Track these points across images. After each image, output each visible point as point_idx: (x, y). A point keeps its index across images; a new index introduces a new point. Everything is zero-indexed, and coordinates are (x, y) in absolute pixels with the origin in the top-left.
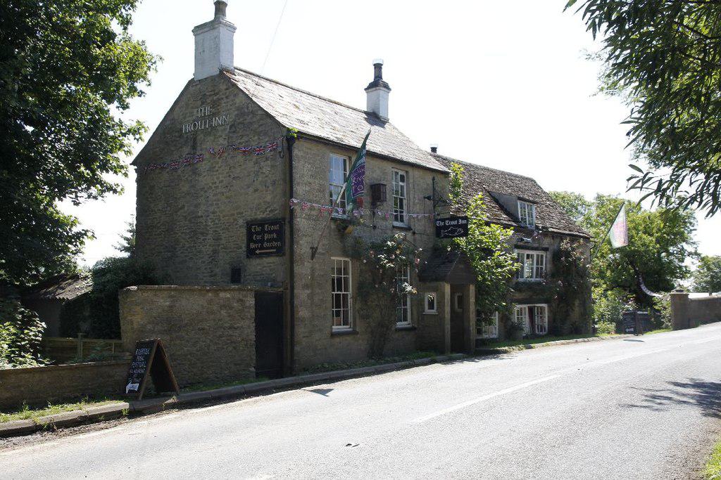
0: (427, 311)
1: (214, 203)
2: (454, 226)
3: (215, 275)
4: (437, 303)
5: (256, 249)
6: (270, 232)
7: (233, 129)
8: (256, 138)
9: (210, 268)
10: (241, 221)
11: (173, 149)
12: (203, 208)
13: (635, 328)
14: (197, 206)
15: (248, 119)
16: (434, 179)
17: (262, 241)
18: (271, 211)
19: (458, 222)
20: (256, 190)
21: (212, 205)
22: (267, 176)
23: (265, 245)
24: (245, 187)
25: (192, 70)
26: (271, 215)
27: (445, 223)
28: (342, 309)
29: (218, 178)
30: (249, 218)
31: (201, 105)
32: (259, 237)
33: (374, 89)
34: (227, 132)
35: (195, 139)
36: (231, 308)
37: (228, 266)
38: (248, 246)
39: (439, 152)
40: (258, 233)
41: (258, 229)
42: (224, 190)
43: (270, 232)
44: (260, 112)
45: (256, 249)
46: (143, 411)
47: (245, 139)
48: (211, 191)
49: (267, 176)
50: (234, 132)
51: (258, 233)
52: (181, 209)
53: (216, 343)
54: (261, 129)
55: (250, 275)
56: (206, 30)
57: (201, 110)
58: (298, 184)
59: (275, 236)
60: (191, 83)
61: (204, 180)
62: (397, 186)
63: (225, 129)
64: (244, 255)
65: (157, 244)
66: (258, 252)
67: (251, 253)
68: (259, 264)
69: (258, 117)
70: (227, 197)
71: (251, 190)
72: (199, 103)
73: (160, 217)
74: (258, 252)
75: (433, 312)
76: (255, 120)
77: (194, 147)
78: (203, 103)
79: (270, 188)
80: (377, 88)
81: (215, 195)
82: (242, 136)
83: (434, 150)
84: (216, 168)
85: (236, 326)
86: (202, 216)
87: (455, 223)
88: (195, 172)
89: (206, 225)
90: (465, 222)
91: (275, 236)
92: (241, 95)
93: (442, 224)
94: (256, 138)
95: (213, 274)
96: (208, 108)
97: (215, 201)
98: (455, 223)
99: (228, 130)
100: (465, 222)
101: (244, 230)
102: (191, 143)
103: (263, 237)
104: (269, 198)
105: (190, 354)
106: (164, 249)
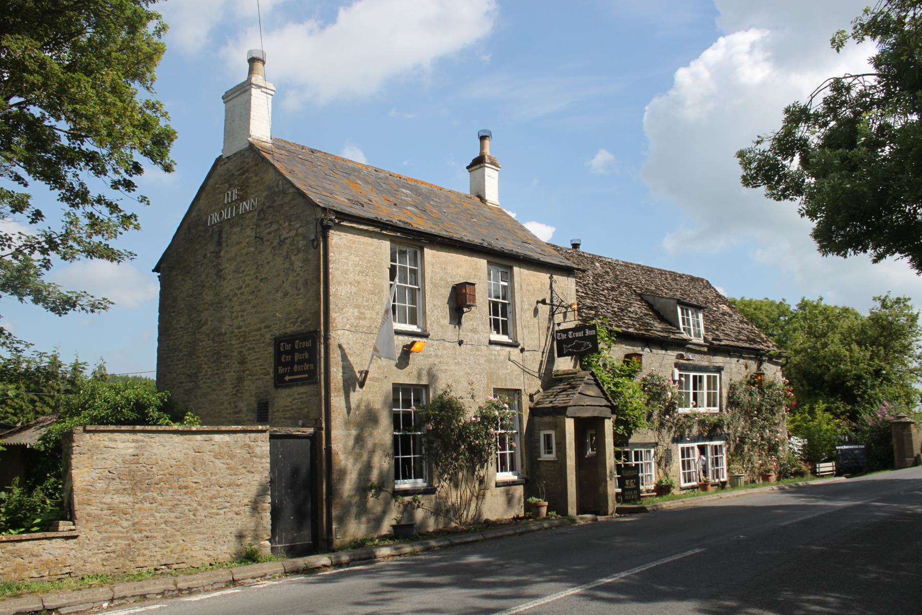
0: (545, 457)
1: (240, 314)
2: (579, 338)
3: (240, 411)
4: (557, 444)
5: (284, 375)
6: (301, 351)
7: (262, 216)
8: (287, 224)
9: (234, 402)
10: (268, 337)
11: (197, 247)
12: (228, 321)
13: (853, 453)
14: (221, 320)
15: (279, 201)
16: (551, 278)
17: (291, 363)
18: (303, 322)
19: (584, 333)
20: (286, 294)
21: (237, 317)
22: (298, 274)
23: (296, 368)
24: (274, 291)
25: (221, 146)
26: (303, 328)
27: (567, 336)
28: (412, 456)
29: (244, 282)
30: (277, 333)
31: (228, 189)
32: (289, 358)
33: (478, 166)
34: (254, 220)
35: (221, 232)
36: (232, 457)
37: (253, 398)
38: (276, 370)
39: (582, 249)
40: (287, 353)
41: (288, 347)
42: (250, 297)
43: (301, 351)
44: (291, 190)
45: (284, 375)
46: (147, 596)
47: (274, 227)
48: (235, 299)
49: (298, 274)
50: (262, 219)
51: (287, 353)
52: (204, 325)
53: (206, 506)
54: (291, 212)
55: (278, 411)
56: (413, 183)
57: (228, 194)
58: (339, 283)
59: (306, 355)
60: (219, 160)
61: (230, 285)
62: (497, 286)
63: (253, 216)
64: (271, 383)
65: (178, 372)
66: (287, 378)
67: (280, 382)
68: (289, 396)
69: (290, 198)
70: (253, 307)
71: (280, 294)
72: (227, 185)
73: (182, 336)
74: (287, 378)
75: (552, 457)
76: (286, 200)
77: (219, 243)
78: (230, 186)
79: (302, 291)
80: (482, 165)
81: (241, 304)
82: (271, 223)
83: (576, 246)
84: (242, 269)
85: (239, 482)
86: (226, 333)
87: (580, 334)
88: (219, 274)
89: (231, 344)
90: (593, 332)
91: (306, 355)
92: (271, 171)
93: (564, 336)
94: (287, 224)
95: (237, 410)
96: (235, 191)
97: (240, 311)
98: (580, 334)
99: (256, 217)
100: (593, 332)
101: (271, 349)
102: (216, 238)
103: (293, 358)
104: (300, 303)
105: (166, 522)
106: (186, 378)
